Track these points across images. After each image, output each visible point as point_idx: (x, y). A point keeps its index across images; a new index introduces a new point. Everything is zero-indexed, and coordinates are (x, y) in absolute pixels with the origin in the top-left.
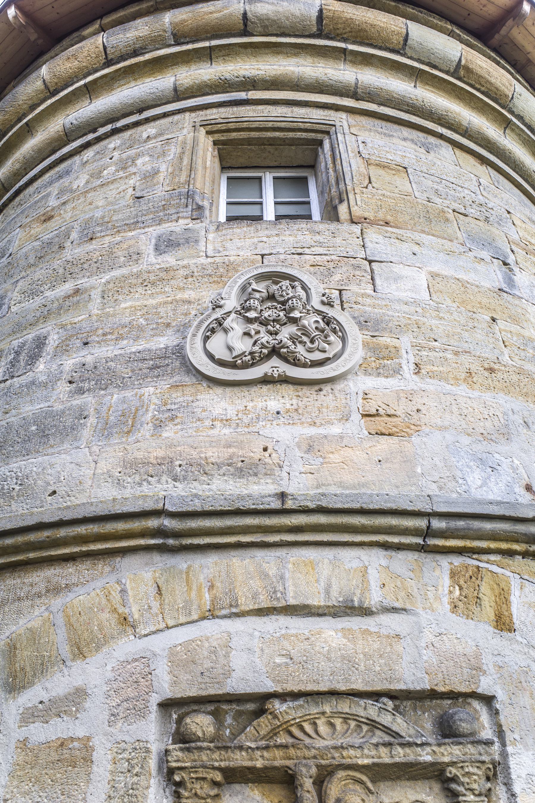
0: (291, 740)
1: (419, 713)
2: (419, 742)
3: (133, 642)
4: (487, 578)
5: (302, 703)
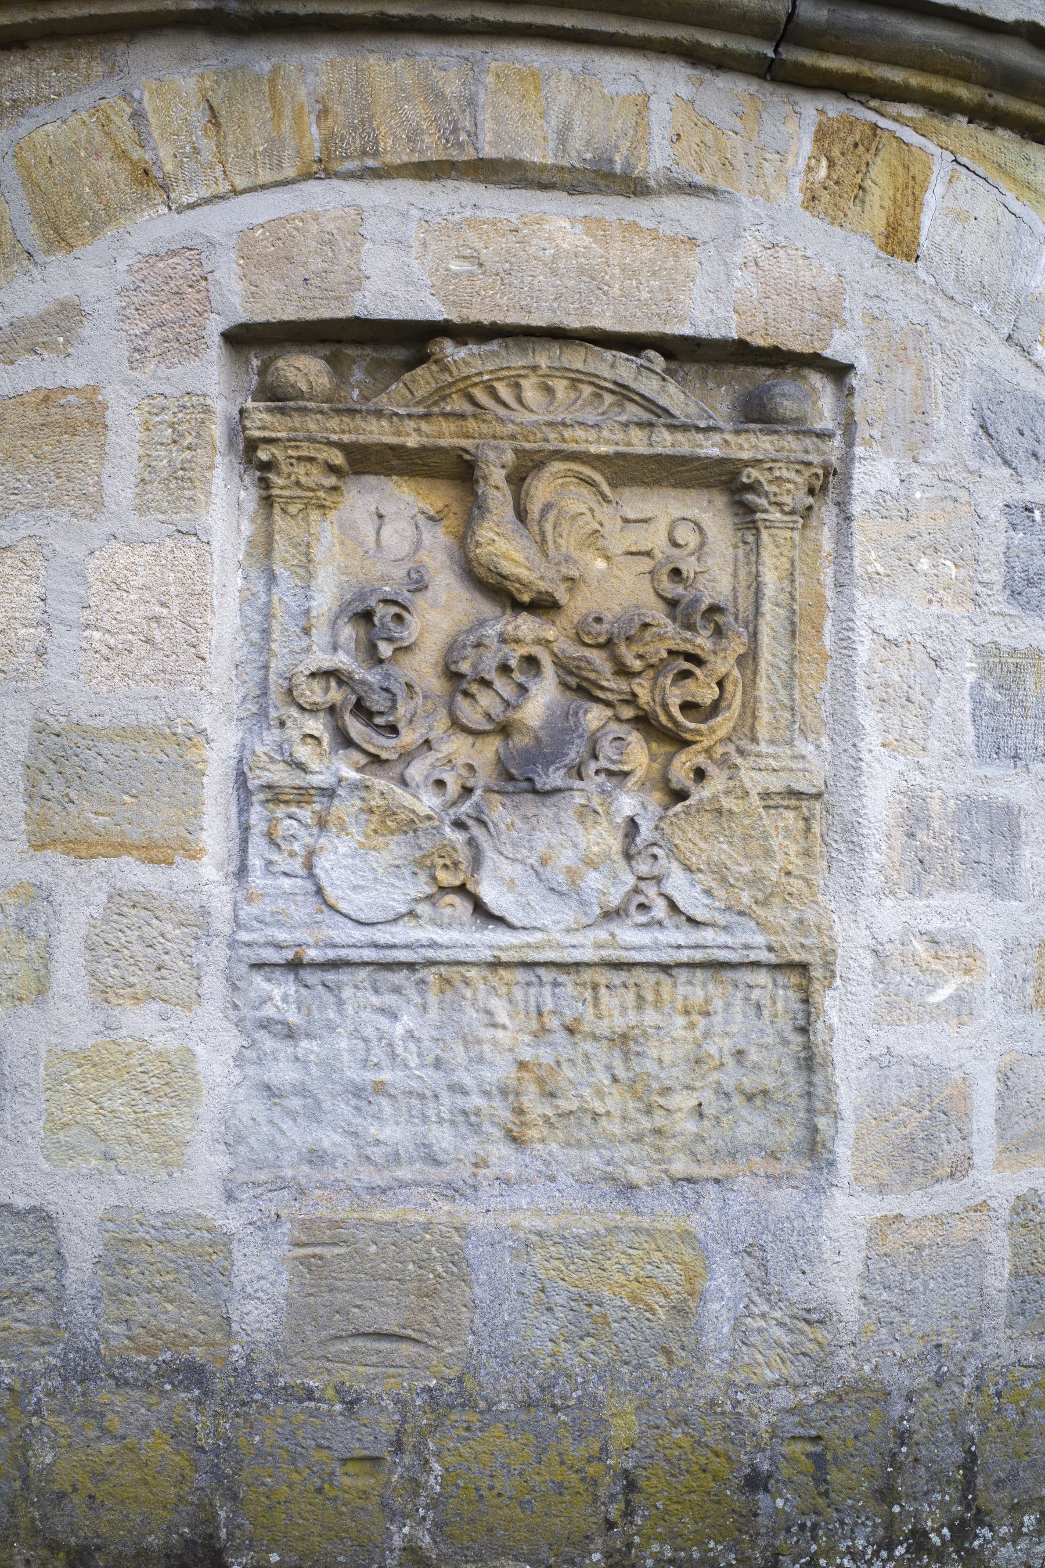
0: (467, 408)
3: (166, 218)
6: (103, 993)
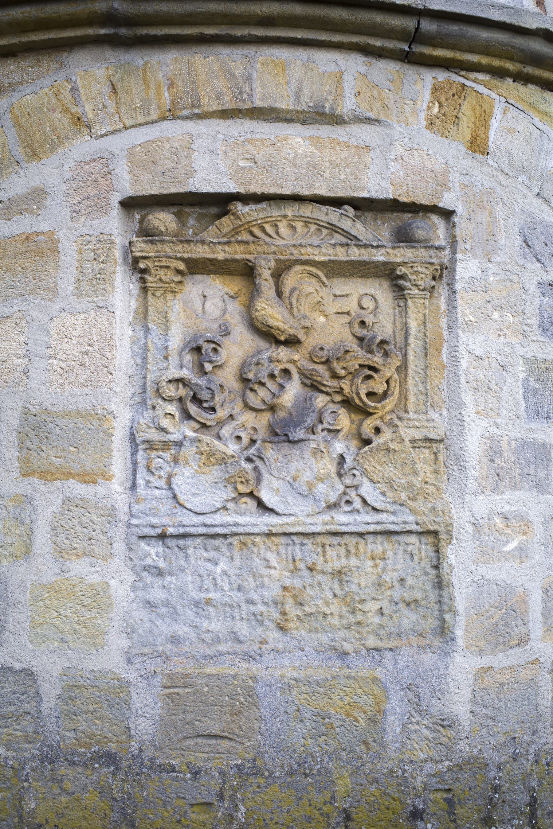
0: (250, 238)
1: (379, 223)
2: (375, 245)
4: (471, 98)
5: (264, 206)
6: (60, 553)
